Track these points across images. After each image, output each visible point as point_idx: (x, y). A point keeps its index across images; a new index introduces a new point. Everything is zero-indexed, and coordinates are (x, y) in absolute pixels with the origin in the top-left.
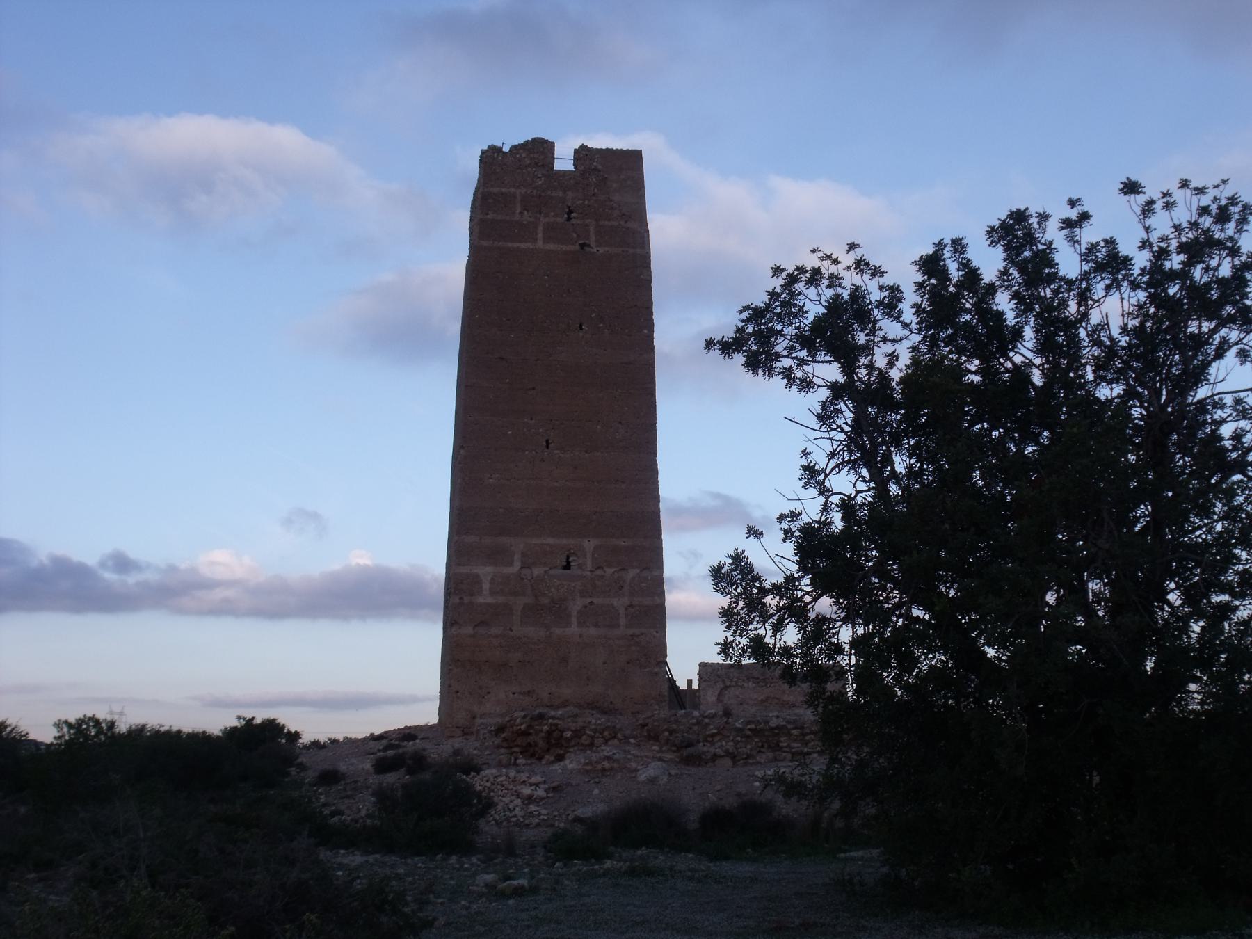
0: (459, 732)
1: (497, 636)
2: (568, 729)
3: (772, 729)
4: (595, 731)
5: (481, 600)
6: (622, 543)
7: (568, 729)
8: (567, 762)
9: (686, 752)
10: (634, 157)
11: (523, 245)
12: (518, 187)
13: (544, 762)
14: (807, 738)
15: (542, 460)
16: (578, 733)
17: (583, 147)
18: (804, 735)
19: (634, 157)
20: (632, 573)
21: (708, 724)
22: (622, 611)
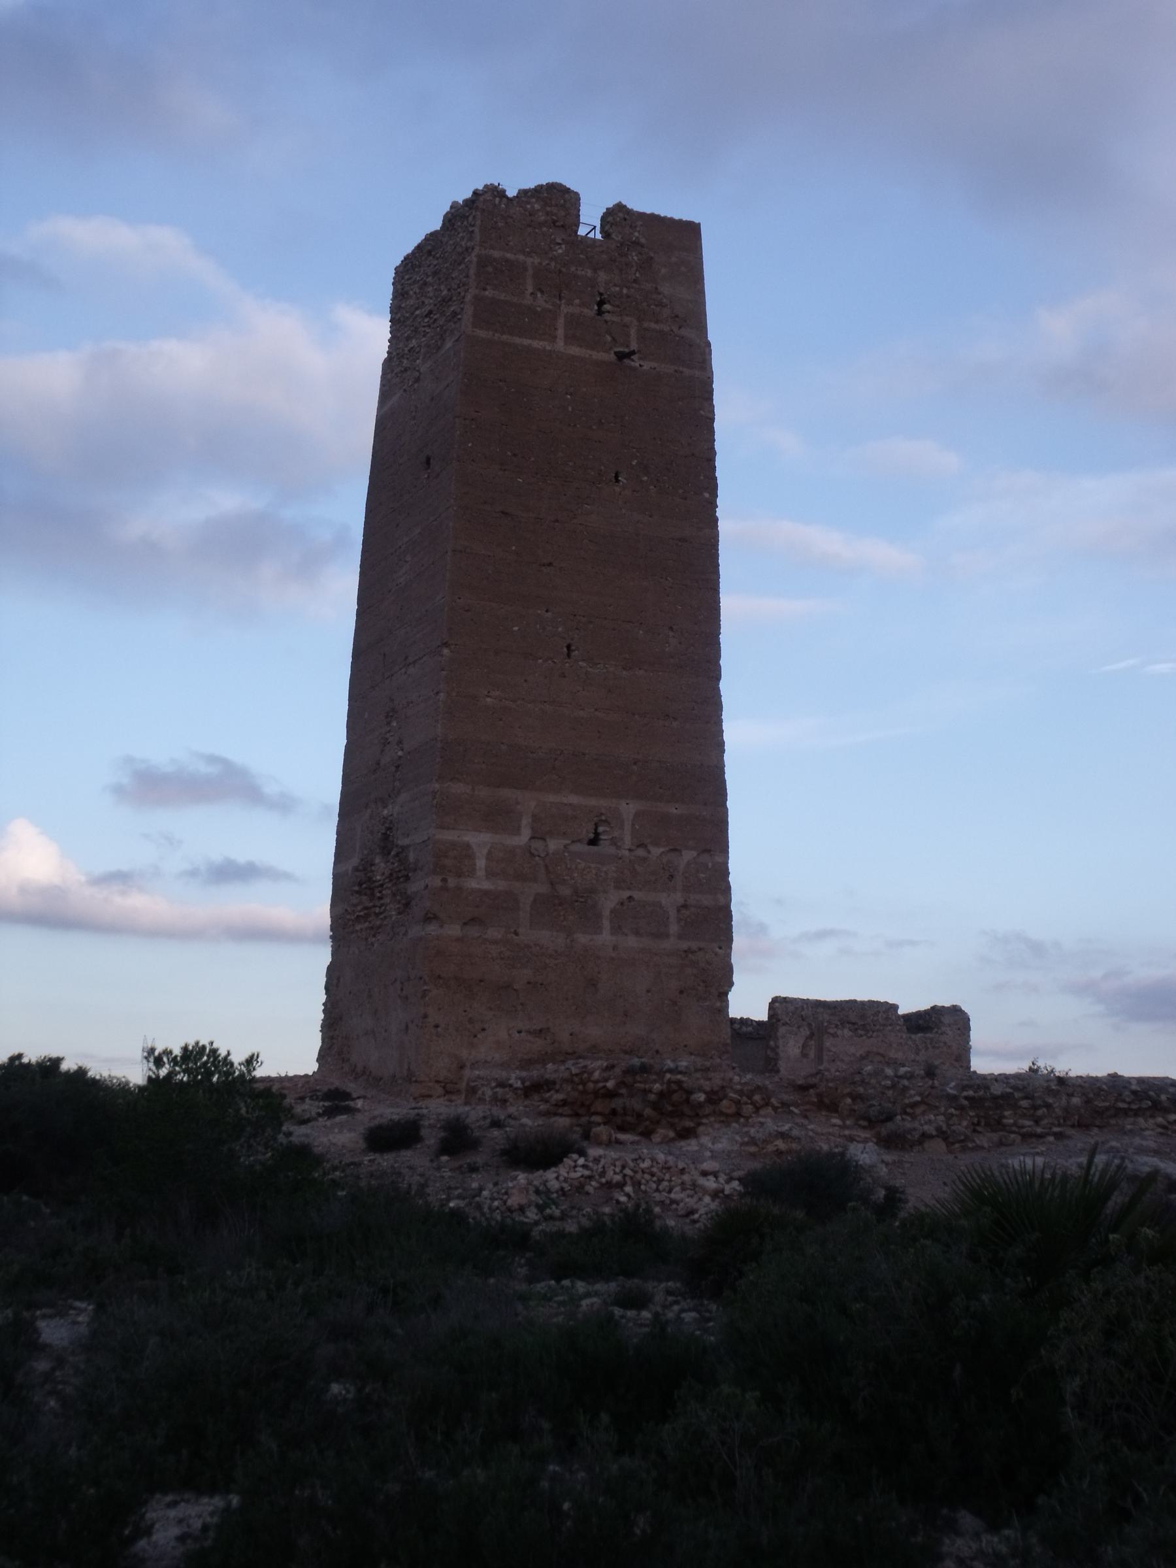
0: (439, 1090)
1: (495, 942)
2: (701, 1089)
3: (995, 1098)
4: (741, 1093)
5: (472, 884)
6: (674, 810)
7: (701, 1089)
8: (705, 1140)
9: (884, 1130)
10: (691, 231)
11: (536, 344)
12: (529, 254)
13: (656, 1138)
14: (1040, 1112)
15: (563, 676)
16: (714, 1097)
17: (620, 207)
18: (1035, 1108)
19: (691, 231)
20: (688, 855)
21: (905, 1089)
22: (673, 913)
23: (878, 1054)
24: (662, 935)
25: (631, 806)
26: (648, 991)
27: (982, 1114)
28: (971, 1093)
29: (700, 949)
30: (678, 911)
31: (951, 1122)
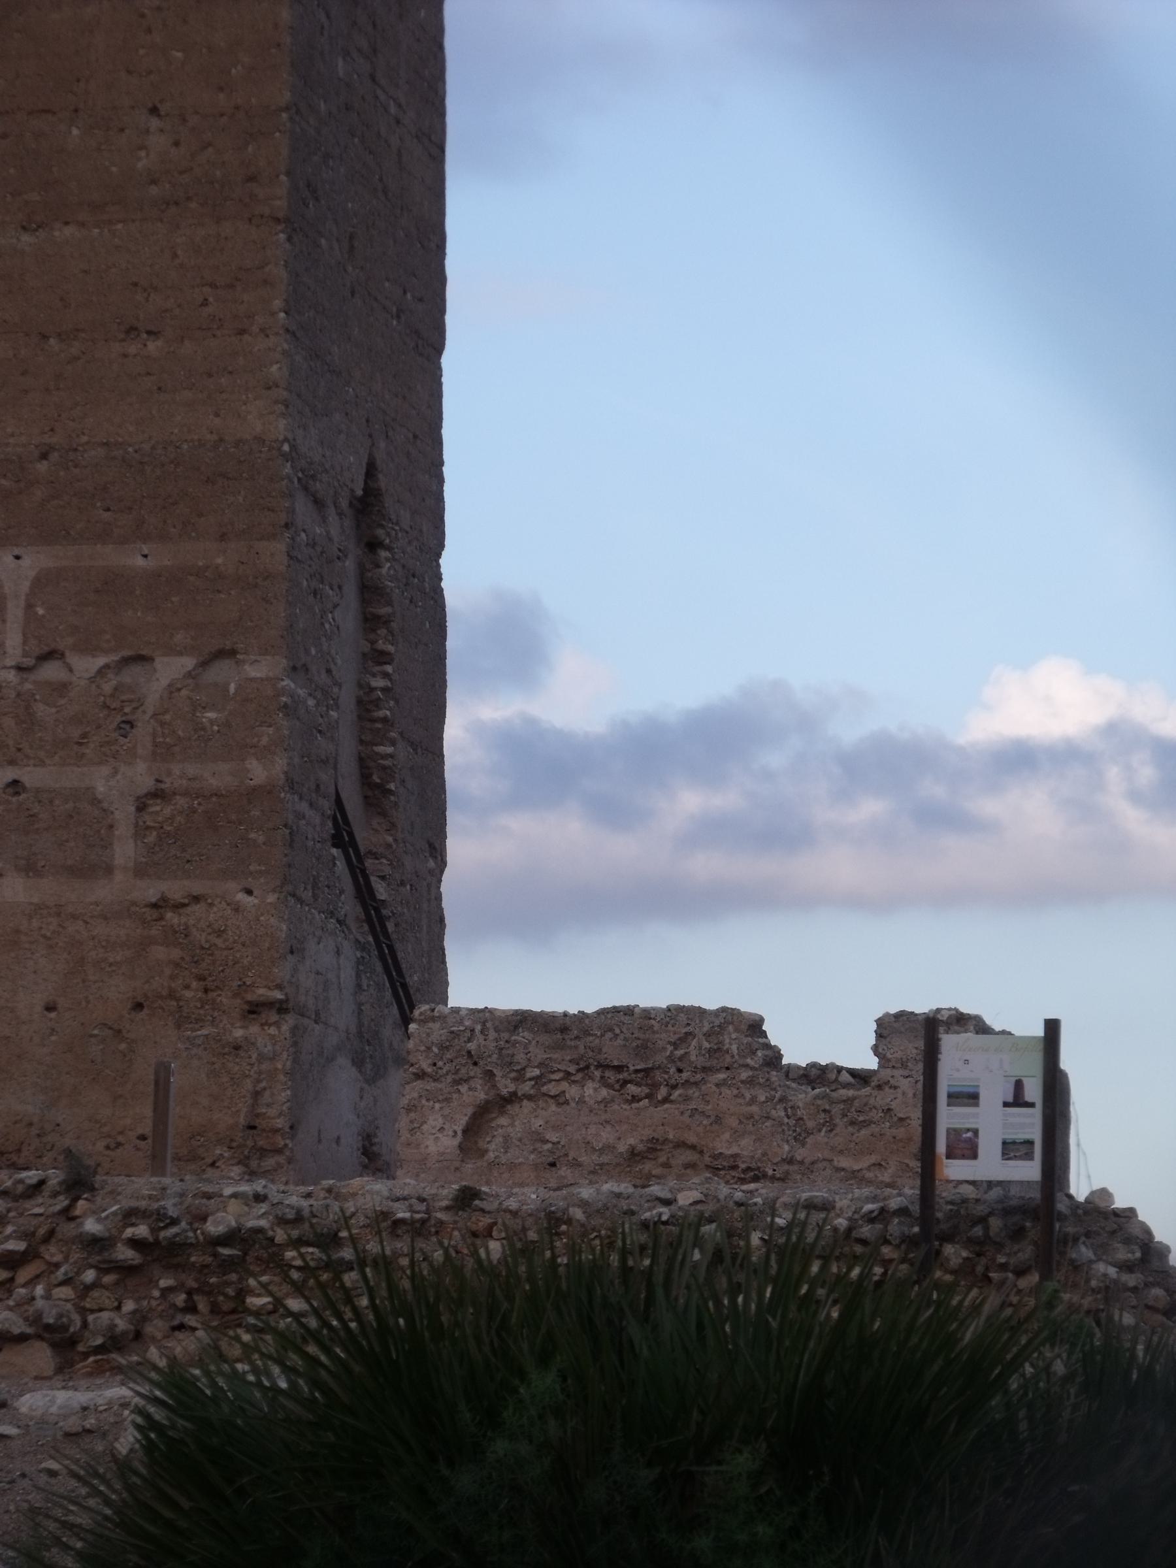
6: (137, 560)
20: (170, 669)
22: (124, 814)
23: (681, 1145)
24: (93, 868)
25: (26, 562)
26: (50, 1008)
27: (192, 1283)
28: (142, 1231)
29: (196, 899)
30: (141, 808)
31: (88, 1304)
